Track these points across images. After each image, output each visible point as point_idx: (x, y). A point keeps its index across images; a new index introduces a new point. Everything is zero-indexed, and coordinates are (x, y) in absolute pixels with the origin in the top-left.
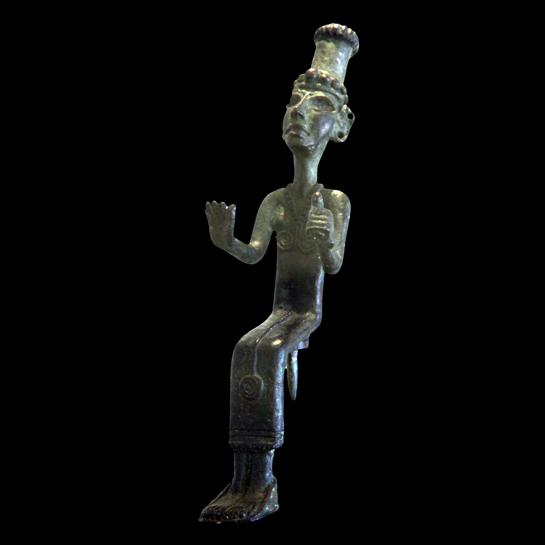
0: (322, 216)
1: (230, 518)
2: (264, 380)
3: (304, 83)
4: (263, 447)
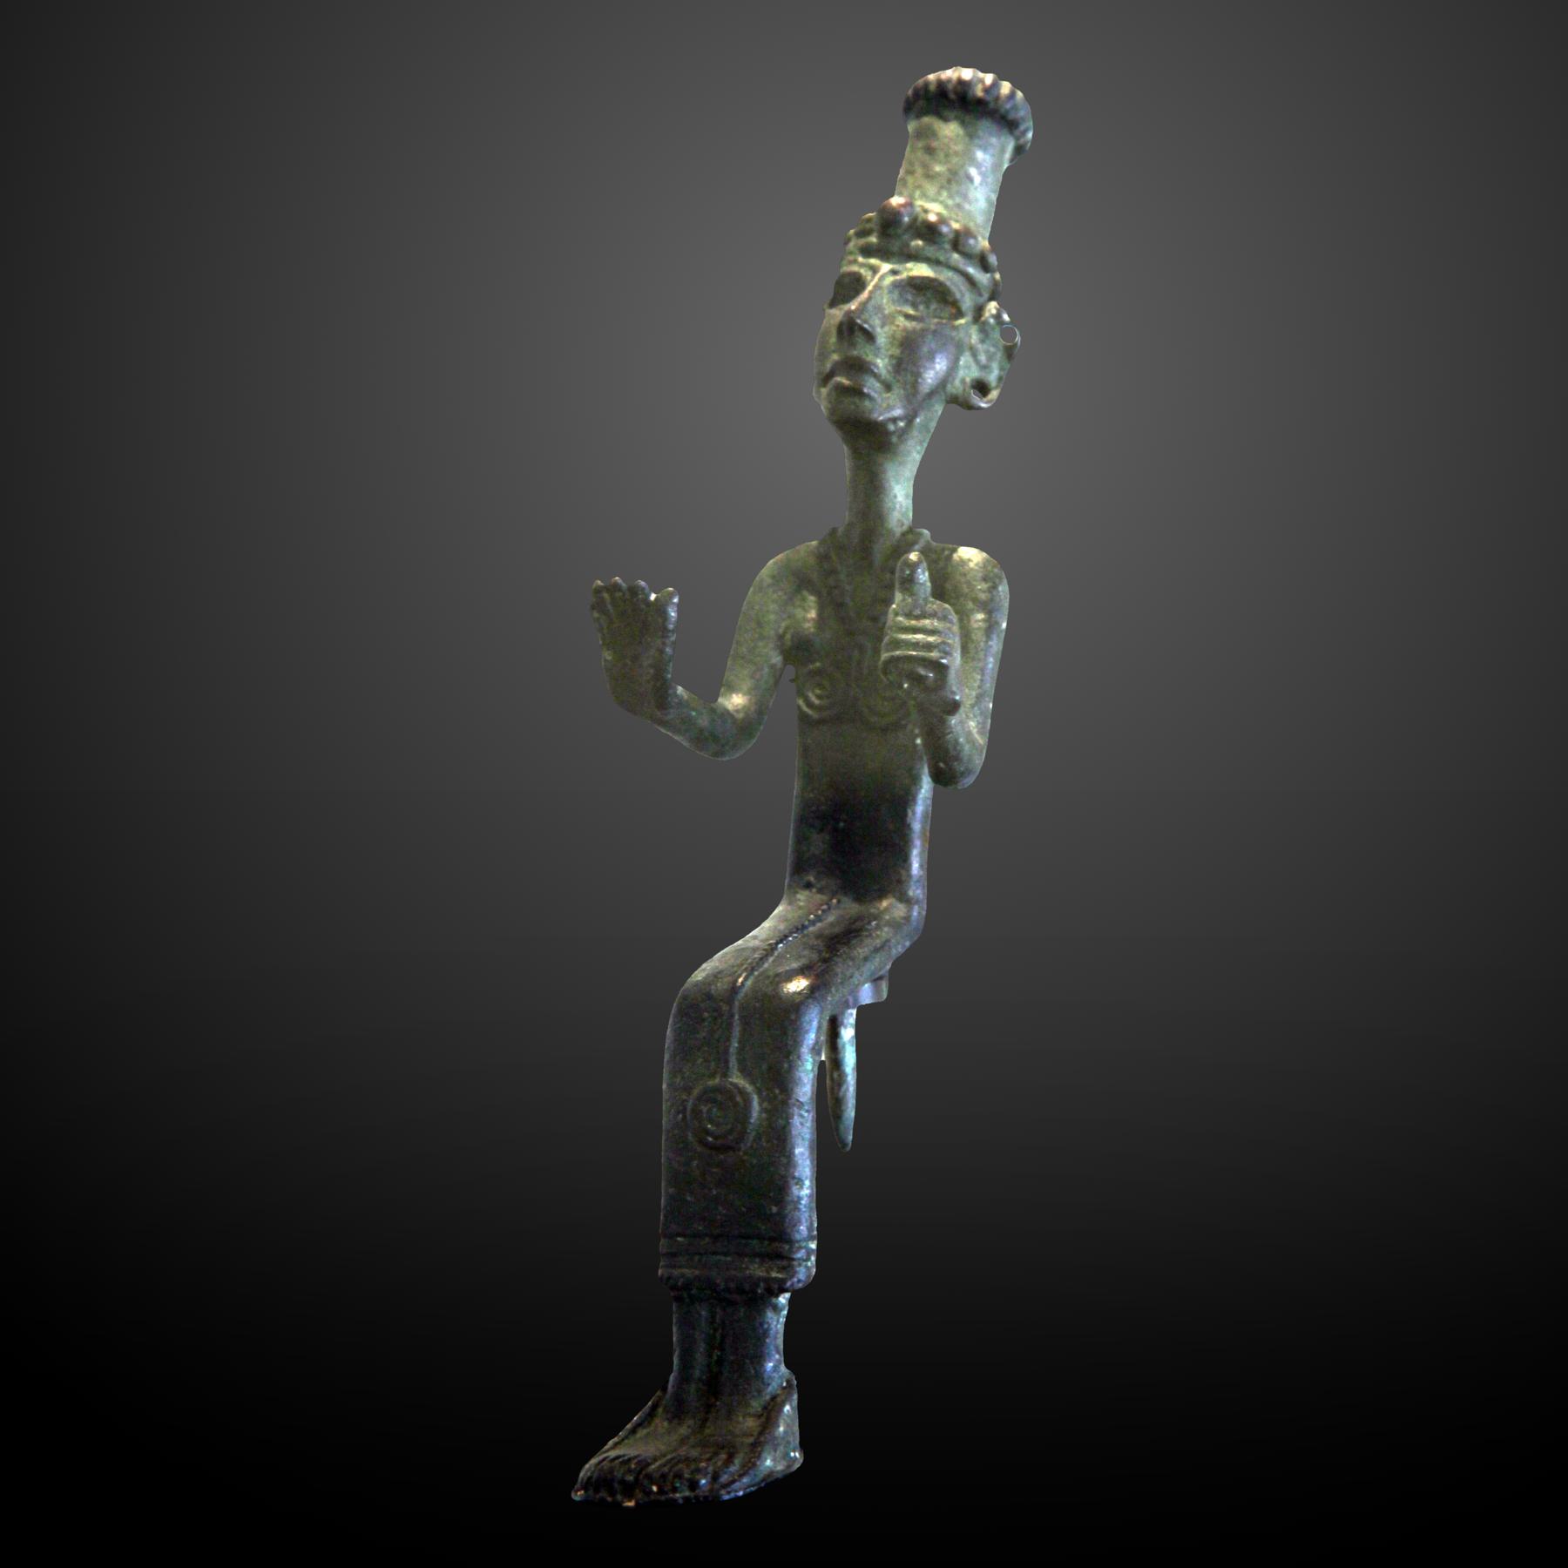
0: (927, 622)
1: (661, 1491)
2: (759, 1092)
3: (873, 239)
4: (757, 1286)
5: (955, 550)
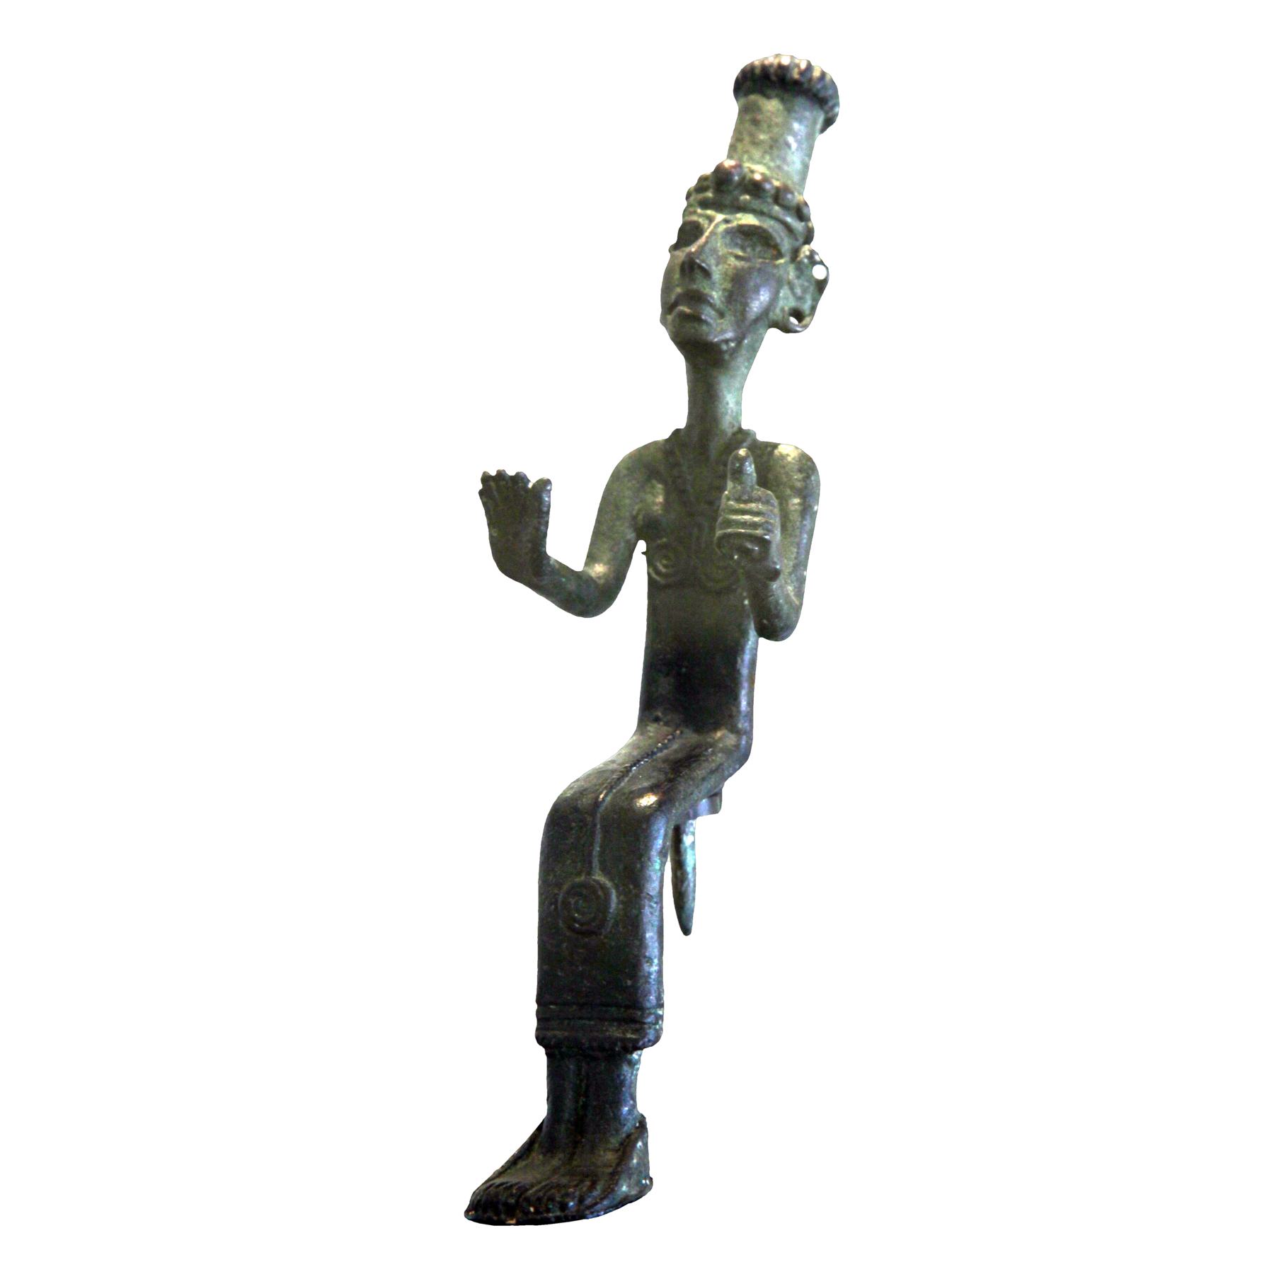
0: (753, 505)
2: (617, 887)
4: (615, 1045)
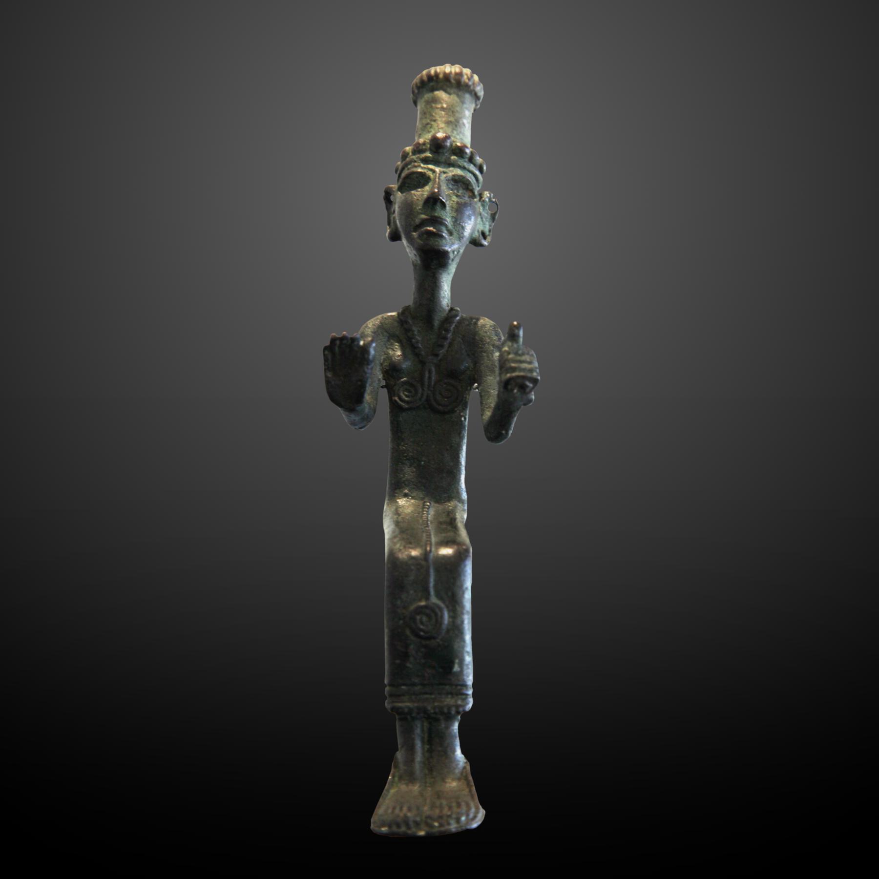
1: (441, 825)
2: (447, 607)
3: (428, 154)
5: (478, 320)
